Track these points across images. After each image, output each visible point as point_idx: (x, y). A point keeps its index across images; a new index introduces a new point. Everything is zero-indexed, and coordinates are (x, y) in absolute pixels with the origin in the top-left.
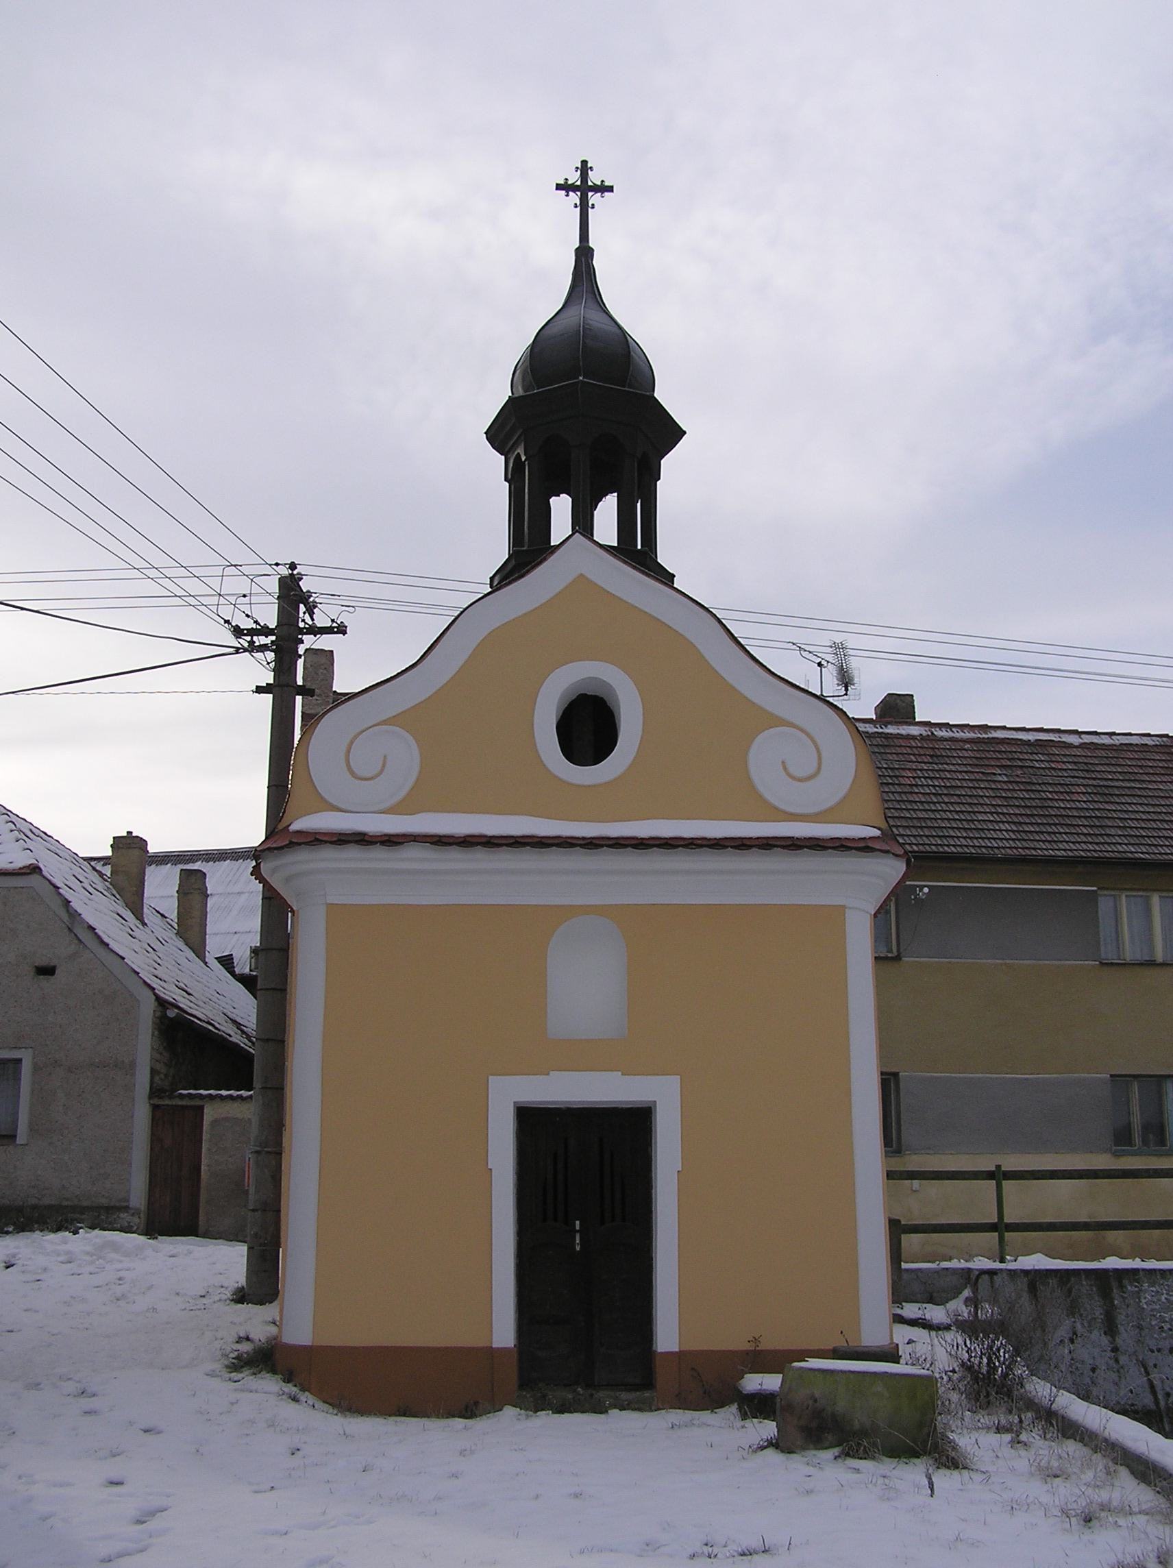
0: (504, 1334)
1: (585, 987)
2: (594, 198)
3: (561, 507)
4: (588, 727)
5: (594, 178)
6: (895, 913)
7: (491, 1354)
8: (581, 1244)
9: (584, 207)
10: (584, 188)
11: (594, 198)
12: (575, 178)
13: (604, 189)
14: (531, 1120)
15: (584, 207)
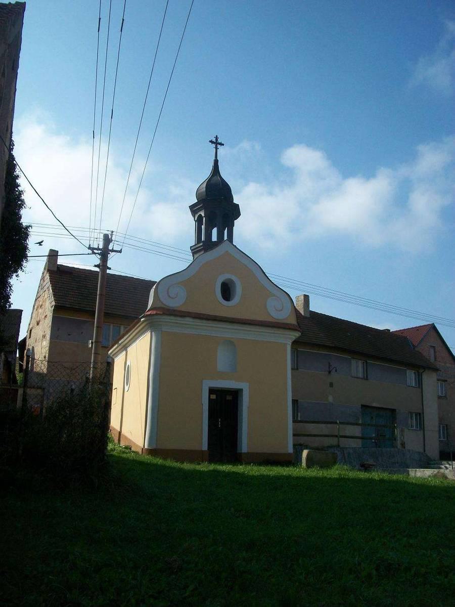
0: (205, 447)
1: (222, 359)
2: (219, 146)
3: (215, 231)
4: (227, 291)
5: (219, 141)
6: (295, 343)
7: (202, 451)
8: (218, 422)
9: (217, 148)
10: (216, 143)
11: (219, 146)
12: (214, 140)
13: (222, 144)
14: (212, 391)
15: (217, 148)
